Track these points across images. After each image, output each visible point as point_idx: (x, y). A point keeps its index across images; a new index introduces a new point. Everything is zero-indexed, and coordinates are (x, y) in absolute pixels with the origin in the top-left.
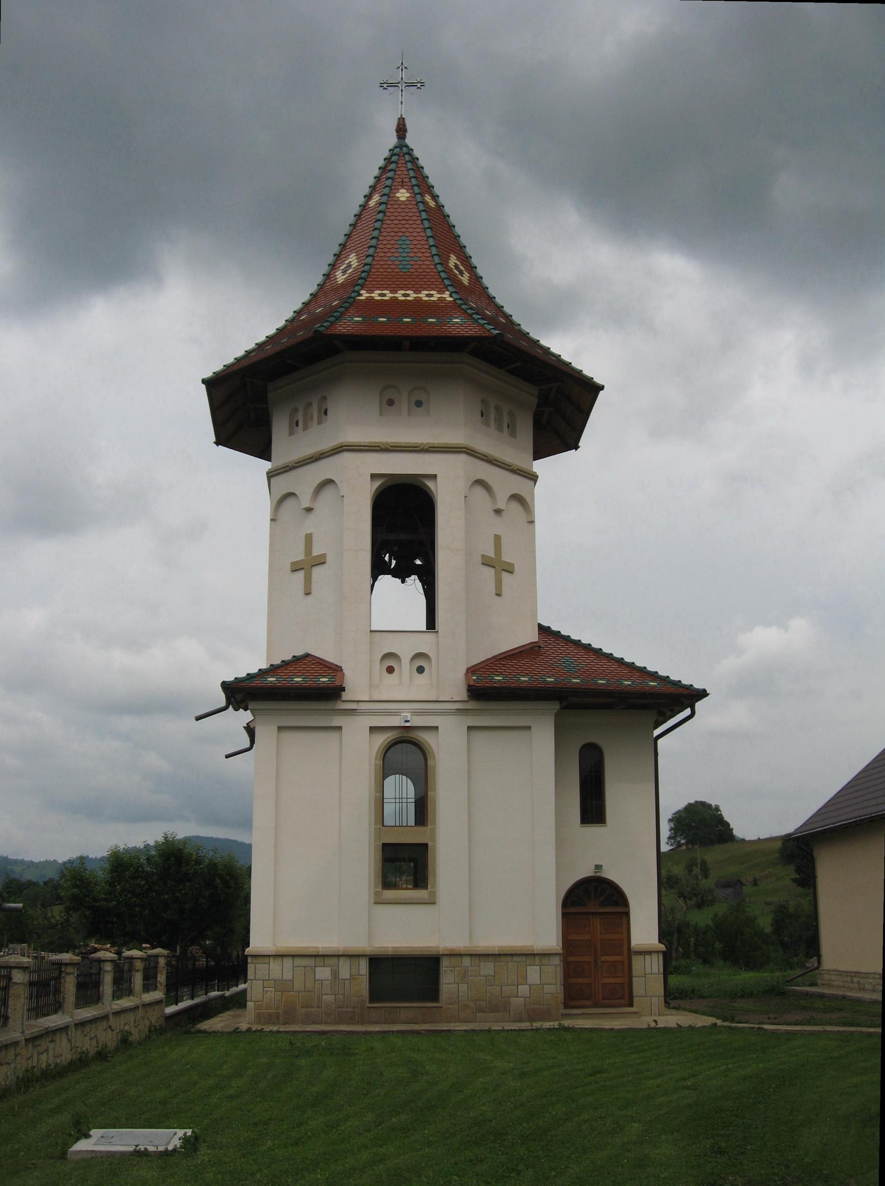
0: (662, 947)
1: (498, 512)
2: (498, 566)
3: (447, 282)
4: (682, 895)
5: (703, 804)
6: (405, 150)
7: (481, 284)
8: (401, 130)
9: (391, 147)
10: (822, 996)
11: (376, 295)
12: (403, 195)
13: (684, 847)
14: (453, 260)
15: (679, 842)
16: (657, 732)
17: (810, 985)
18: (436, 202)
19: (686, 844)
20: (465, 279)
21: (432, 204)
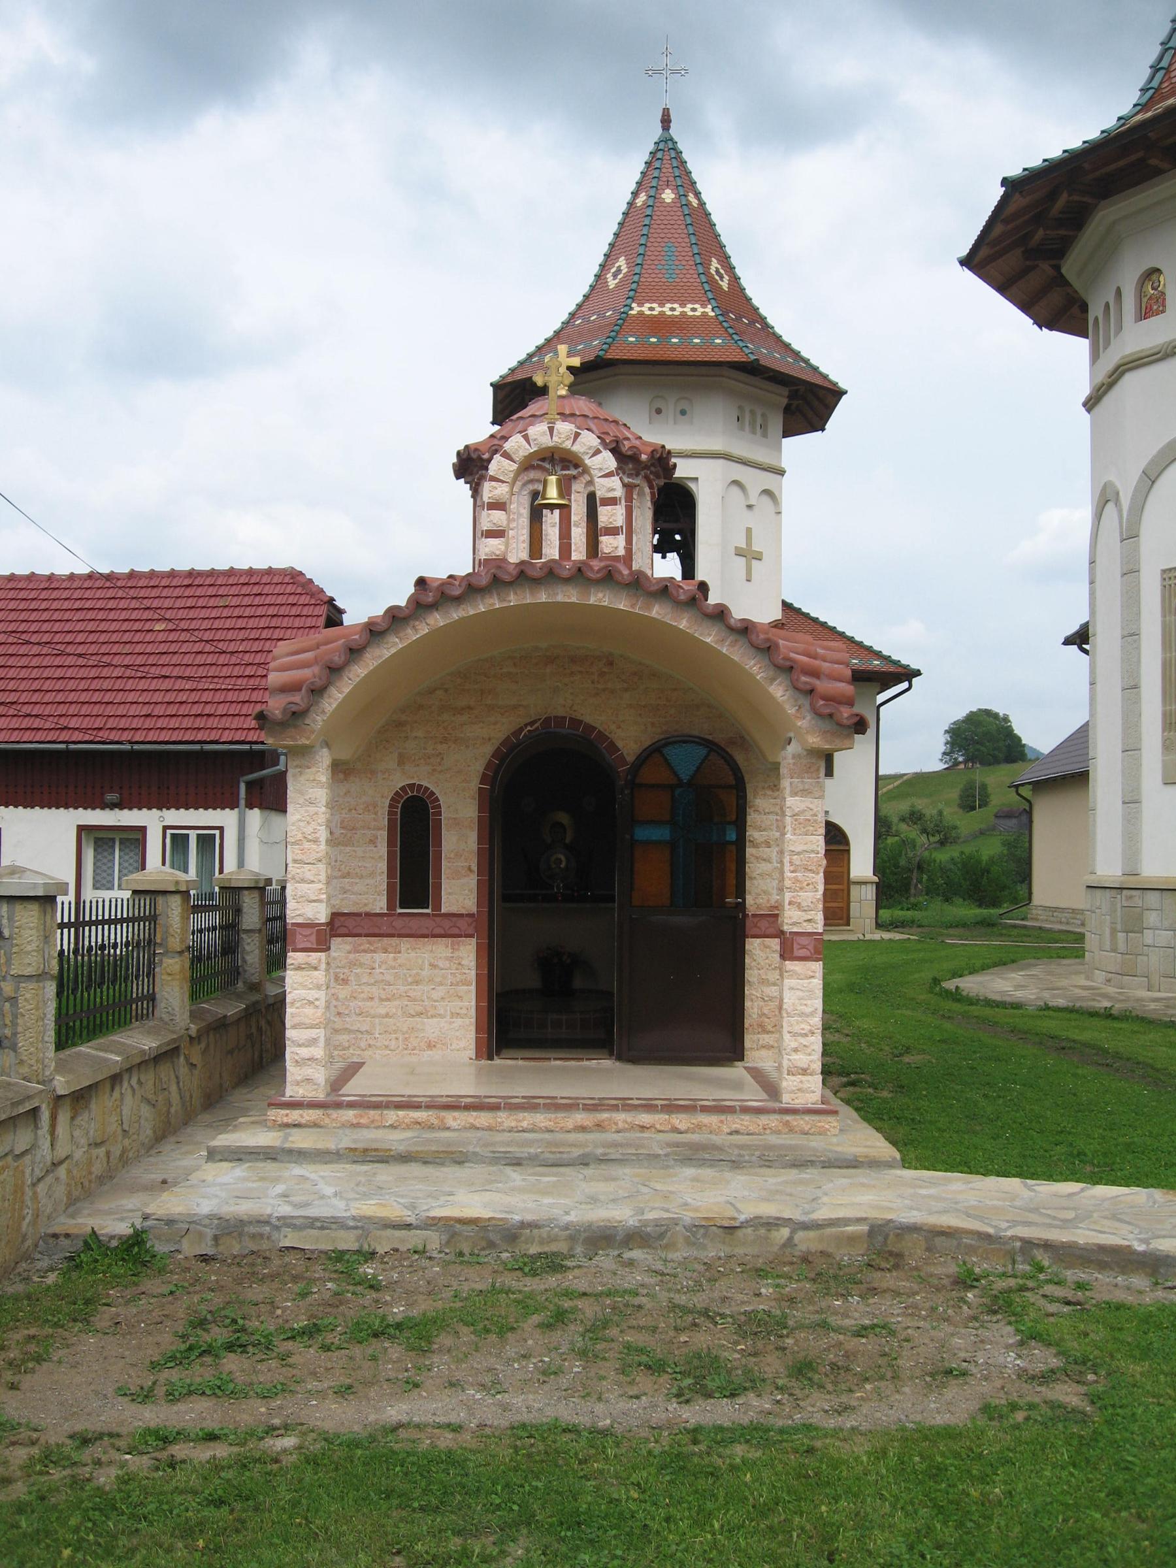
0: (876, 879)
1: (750, 507)
2: (749, 555)
3: (710, 295)
4: (924, 831)
5: (988, 712)
6: (670, 145)
7: (739, 285)
8: (666, 121)
9: (656, 140)
10: (1025, 927)
11: (645, 309)
12: (668, 196)
13: (962, 766)
14: (715, 264)
15: (956, 759)
16: (881, 698)
19: (965, 762)
20: (725, 285)
21: (695, 202)
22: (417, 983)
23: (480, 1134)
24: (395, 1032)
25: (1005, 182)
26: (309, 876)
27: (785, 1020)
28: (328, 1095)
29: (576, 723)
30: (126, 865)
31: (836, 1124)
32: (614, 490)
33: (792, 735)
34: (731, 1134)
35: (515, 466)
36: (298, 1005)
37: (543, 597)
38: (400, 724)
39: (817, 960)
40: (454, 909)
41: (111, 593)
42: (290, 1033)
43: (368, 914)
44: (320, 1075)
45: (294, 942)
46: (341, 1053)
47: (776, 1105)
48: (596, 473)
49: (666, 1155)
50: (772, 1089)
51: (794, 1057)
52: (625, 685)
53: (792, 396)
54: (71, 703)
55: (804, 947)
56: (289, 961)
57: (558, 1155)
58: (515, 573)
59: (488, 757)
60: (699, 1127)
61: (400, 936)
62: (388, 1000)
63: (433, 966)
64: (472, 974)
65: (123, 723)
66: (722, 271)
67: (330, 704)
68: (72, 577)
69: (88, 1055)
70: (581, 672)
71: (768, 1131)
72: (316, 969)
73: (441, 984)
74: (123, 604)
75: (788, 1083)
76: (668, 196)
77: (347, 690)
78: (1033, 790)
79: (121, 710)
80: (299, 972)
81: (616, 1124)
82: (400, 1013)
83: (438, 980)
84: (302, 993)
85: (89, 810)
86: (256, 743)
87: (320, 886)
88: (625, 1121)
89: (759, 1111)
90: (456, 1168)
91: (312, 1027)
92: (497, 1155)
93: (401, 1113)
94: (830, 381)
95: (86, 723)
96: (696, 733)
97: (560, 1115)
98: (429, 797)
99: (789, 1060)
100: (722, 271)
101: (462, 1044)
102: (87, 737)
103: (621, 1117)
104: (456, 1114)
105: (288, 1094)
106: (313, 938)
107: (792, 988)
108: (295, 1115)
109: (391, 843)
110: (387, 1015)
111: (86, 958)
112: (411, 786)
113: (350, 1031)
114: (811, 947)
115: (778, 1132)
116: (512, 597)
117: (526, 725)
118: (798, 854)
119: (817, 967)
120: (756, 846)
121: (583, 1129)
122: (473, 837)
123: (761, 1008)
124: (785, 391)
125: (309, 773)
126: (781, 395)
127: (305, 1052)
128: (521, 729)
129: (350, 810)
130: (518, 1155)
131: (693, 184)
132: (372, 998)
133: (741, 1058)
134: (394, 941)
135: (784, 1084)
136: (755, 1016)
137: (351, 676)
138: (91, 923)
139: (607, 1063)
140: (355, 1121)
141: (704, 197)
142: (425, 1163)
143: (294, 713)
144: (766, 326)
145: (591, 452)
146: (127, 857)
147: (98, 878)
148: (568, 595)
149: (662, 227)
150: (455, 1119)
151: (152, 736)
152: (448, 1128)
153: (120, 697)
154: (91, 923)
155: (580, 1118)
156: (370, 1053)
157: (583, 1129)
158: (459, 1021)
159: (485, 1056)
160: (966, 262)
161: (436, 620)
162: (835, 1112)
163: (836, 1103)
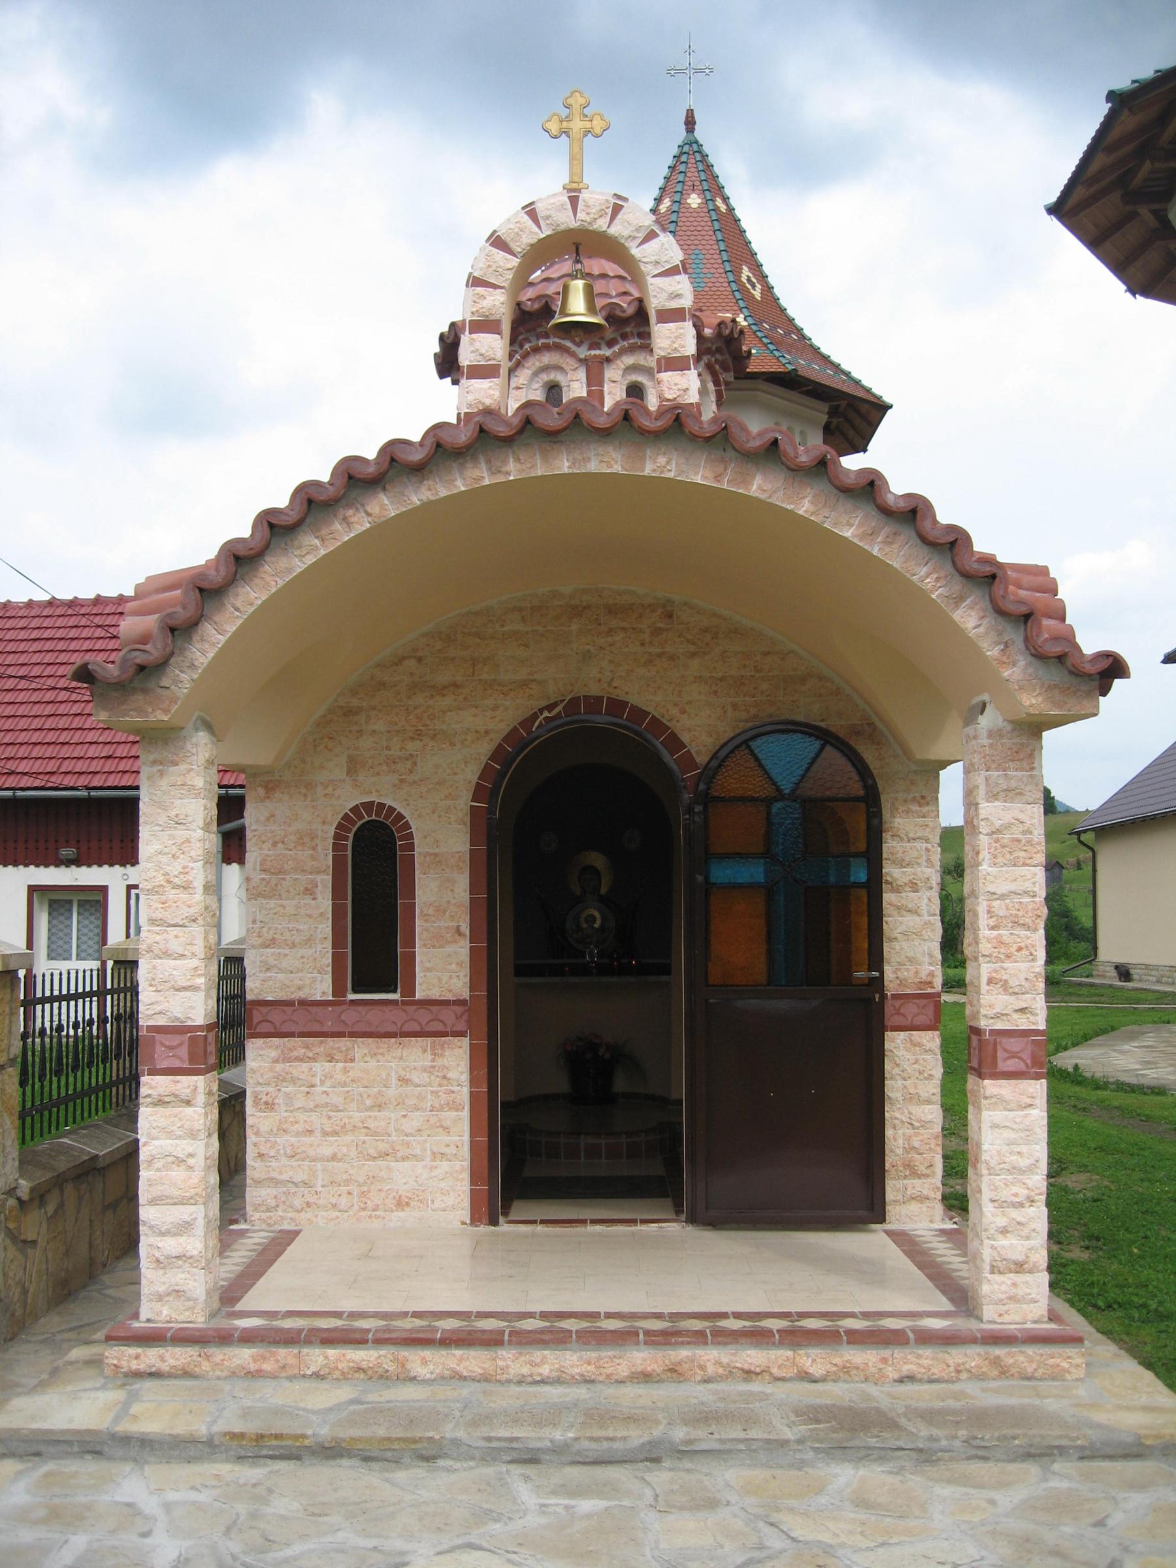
3: (742, 304)
6: (695, 147)
8: (690, 123)
9: (680, 143)
10: (1092, 985)
12: (694, 200)
14: (746, 272)
17: (1087, 977)
18: (727, 205)
20: (757, 293)
21: (723, 208)
22: (380, 1107)
23: (466, 1391)
24: (347, 1182)
25: (1111, 96)
26: (175, 946)
27: (985, 1179)
28: (213, 1315)
29: (617, 706)
30: (86, 931)
31: (1079, 1360)
32: (679, 296)
33: (986, 697)
34: (901, 1381)
35: (515, 262)
36: (159, 1164)
37: (564, 465)
38: (349, 712)
39: (1037, 1077)
40: (435, 994)
41: (72, 621)
42: (147, 1213)
43: (303, 1003)
44: (197, 1285)
45: (152, 1058)
46: (264, 1215)
47: (972, 1325)
48: (648, 269)
49: (800, 1441)
50: (963, 1298)
51: (1003, 1242)
52: (693, 648)
53: (833, 413)
54: (22, 744)
55: (1014, 1055)
56: (143, 1091)
57: (605, 1445)
58: (516, 422)
59: (484, 760)
60: (846, 1370)
61: (353, 1035)
62: (336, 1133)
63: (403, 1081)
64: (463, 1094)
65: (80, 766)
66: (754, 280)
67: (204, 652)
68: (30, 604)
69: (69, 1146)
70: (624, 629)
71: (964, 1376)
72: (188, 1103)
73: (416, 1108)
74: (86, 633)
75: (993, 1288)
76: (694, 200)
77: (231, 628)
78: (1097, 837)
79: (79, 751)
80: (160, 1109)
81: (703, 1368)
82: (354, 1154)
83: (411, 1102)
84: (166, 1144)
85: (42, 868)
86: (233, 786)
87: (195, 962)
88: (718, 1363)
89: (947, 1339)
90: (420, 1471)
91: (183, 1202)
92: (495, 1444)
93: (332, 1352)
94: (874, 395)
95: (38, 766)
96: (800, 718)
97: (607, 1353)
98: (400, 830)
99: (992, 1247)
100: (749, 286)
101: (450, 1200)
102: (37, 783)
103: (712, 1356)
104: (427, 1353)
105: (144, 1314)
106: (184, 1052)
107: (995, 1126)
108: (151, 1357)
109: (337, 892)
110: (334, 1158)
111: (38, 1040)
112: (368, 806)
113: (276, 1182)
114: (1026, 1055)
115: (981, 1377)
116: (512, 466)
117: (541, 711)
118: (1002, 897)
119: (1038, 1089)
120: (897, 890)
121: (645, 1377)
122: (462, 882)
123: (908, 1139)
124: (825, 407)
125: (175, 773)
126: (820, 411)
127: (170, 1245)
128: (534, 717)
129: (275, 844)
130: (533, 1444)
131: (721, 188)
132: (311, 1132)
133: (882, 1219)
134: (344, 1043)
135: (985, 1289)
136: (900, 1151)
137: (238, 603)
138: (43, 1000)
139: (674, 1228)
140: (253, 1367)
141: (732, 202)
142: (367, 1459)
143: (142, 668)
144: (803, 337)
145: (641, 235)
146: (86, 922)
147: (54, 946)
148: (607, 461)
149: (689, 233)
150: (424, 1362)
151: (112, 781)
152: (413, 1379)
153: (77, 737)
154: (43, 1000)
155: (640, 1357)
156: (309, 1215)
157: (645, 1377)
158: (445, 1166)
159: (486, 1218)
160: (1055, 210)
161: (382, 506)
162: (1077, 1340)
163: (1076, 1322)
